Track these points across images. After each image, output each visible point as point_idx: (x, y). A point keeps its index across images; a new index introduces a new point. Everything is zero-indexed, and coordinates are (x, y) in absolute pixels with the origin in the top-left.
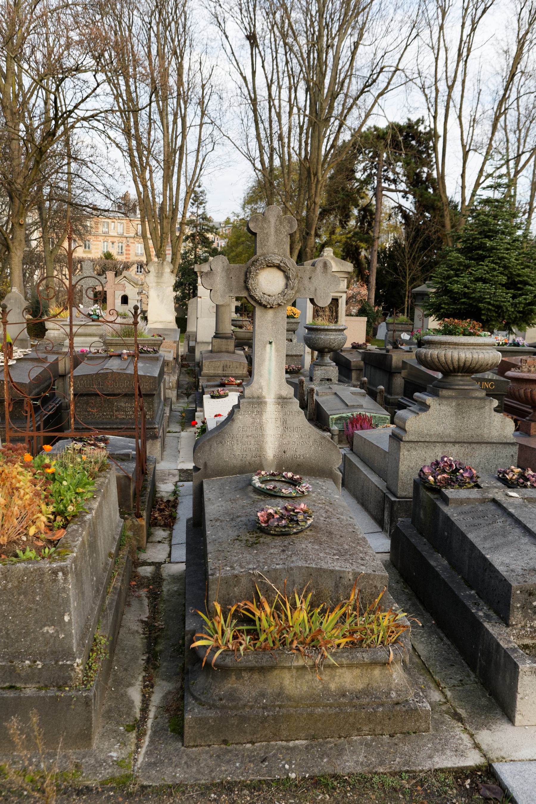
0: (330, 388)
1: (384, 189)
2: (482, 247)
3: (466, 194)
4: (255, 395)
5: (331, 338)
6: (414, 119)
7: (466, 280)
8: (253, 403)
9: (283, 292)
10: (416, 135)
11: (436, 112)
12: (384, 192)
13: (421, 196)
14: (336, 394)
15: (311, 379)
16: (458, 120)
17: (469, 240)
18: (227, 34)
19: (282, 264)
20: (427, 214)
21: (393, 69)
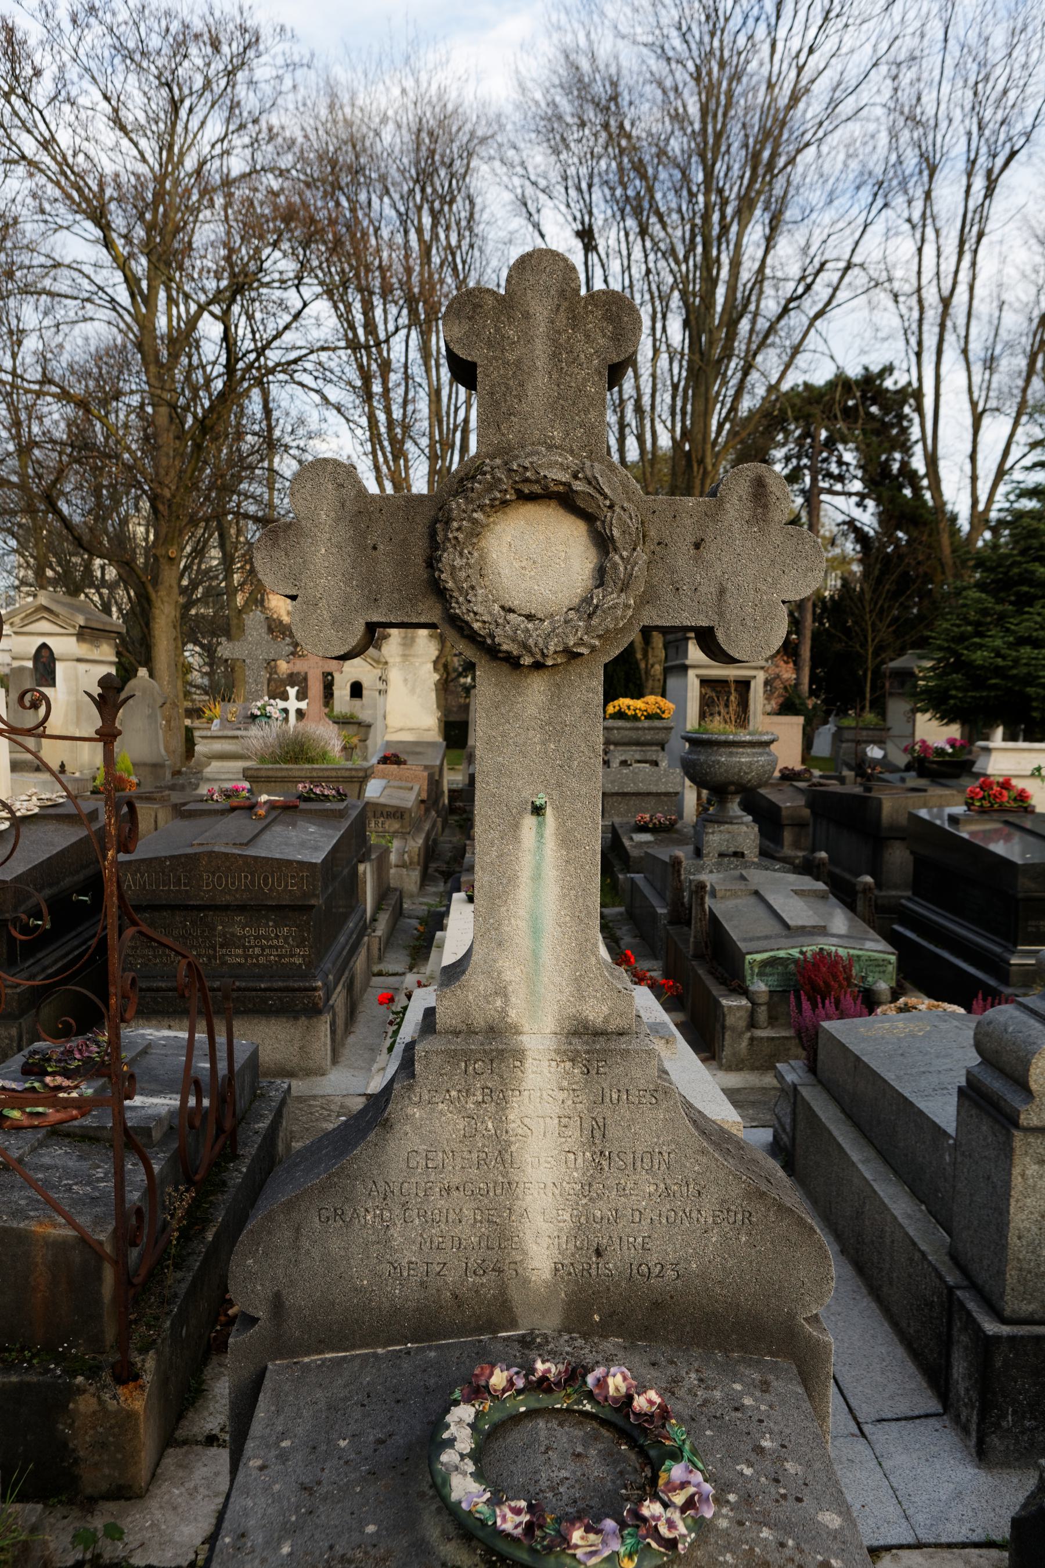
0: (743, 878)
1: (822, 491)
2: (1027, 578)
3: (979, 492)
4: (479, 1022)
5: (744, 762)
6: (875, 369)
7: (998, 643)
8: (467, 1056)
9: (587, 600)
10: (879, 396)
11: (920, 343)
12: (823, 497)
13: (892, 500)
14: (756, 893)
15: (698, 853)
16: (962, 357)
17: (1000, 565)
18: (544, 230)
19: (579, 486)
20: (900, 534)
21: (842, 265)
